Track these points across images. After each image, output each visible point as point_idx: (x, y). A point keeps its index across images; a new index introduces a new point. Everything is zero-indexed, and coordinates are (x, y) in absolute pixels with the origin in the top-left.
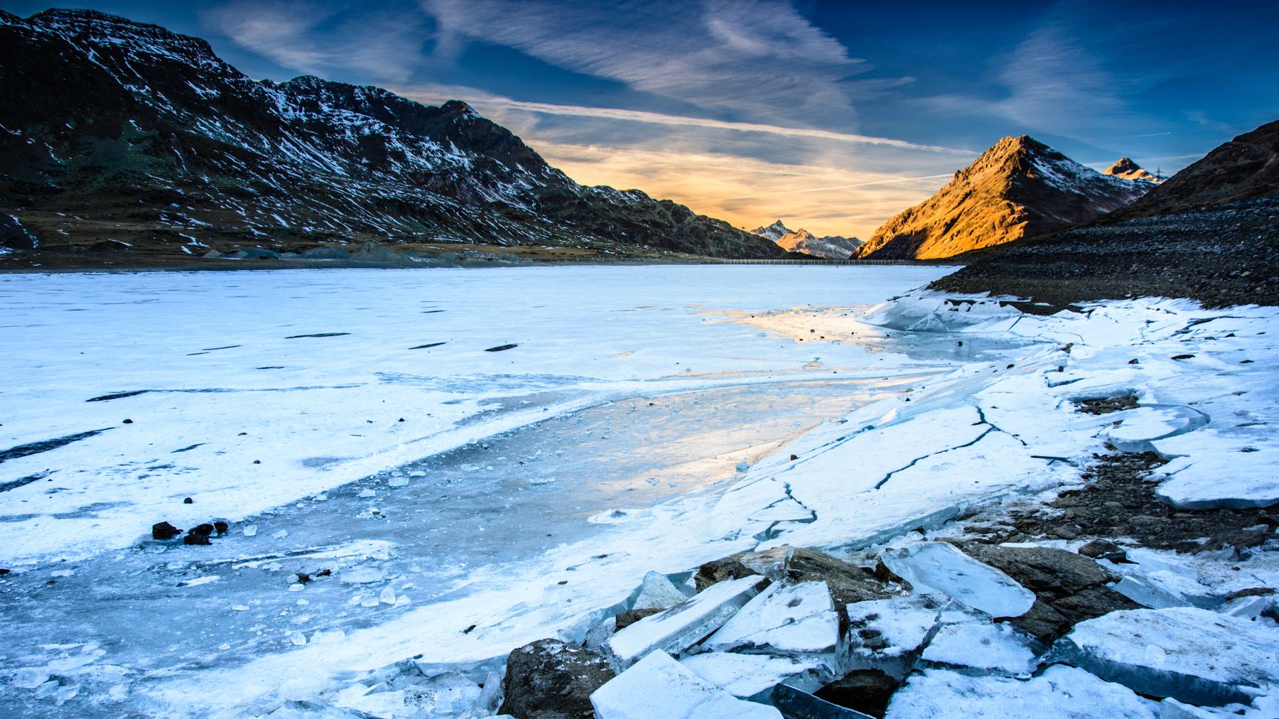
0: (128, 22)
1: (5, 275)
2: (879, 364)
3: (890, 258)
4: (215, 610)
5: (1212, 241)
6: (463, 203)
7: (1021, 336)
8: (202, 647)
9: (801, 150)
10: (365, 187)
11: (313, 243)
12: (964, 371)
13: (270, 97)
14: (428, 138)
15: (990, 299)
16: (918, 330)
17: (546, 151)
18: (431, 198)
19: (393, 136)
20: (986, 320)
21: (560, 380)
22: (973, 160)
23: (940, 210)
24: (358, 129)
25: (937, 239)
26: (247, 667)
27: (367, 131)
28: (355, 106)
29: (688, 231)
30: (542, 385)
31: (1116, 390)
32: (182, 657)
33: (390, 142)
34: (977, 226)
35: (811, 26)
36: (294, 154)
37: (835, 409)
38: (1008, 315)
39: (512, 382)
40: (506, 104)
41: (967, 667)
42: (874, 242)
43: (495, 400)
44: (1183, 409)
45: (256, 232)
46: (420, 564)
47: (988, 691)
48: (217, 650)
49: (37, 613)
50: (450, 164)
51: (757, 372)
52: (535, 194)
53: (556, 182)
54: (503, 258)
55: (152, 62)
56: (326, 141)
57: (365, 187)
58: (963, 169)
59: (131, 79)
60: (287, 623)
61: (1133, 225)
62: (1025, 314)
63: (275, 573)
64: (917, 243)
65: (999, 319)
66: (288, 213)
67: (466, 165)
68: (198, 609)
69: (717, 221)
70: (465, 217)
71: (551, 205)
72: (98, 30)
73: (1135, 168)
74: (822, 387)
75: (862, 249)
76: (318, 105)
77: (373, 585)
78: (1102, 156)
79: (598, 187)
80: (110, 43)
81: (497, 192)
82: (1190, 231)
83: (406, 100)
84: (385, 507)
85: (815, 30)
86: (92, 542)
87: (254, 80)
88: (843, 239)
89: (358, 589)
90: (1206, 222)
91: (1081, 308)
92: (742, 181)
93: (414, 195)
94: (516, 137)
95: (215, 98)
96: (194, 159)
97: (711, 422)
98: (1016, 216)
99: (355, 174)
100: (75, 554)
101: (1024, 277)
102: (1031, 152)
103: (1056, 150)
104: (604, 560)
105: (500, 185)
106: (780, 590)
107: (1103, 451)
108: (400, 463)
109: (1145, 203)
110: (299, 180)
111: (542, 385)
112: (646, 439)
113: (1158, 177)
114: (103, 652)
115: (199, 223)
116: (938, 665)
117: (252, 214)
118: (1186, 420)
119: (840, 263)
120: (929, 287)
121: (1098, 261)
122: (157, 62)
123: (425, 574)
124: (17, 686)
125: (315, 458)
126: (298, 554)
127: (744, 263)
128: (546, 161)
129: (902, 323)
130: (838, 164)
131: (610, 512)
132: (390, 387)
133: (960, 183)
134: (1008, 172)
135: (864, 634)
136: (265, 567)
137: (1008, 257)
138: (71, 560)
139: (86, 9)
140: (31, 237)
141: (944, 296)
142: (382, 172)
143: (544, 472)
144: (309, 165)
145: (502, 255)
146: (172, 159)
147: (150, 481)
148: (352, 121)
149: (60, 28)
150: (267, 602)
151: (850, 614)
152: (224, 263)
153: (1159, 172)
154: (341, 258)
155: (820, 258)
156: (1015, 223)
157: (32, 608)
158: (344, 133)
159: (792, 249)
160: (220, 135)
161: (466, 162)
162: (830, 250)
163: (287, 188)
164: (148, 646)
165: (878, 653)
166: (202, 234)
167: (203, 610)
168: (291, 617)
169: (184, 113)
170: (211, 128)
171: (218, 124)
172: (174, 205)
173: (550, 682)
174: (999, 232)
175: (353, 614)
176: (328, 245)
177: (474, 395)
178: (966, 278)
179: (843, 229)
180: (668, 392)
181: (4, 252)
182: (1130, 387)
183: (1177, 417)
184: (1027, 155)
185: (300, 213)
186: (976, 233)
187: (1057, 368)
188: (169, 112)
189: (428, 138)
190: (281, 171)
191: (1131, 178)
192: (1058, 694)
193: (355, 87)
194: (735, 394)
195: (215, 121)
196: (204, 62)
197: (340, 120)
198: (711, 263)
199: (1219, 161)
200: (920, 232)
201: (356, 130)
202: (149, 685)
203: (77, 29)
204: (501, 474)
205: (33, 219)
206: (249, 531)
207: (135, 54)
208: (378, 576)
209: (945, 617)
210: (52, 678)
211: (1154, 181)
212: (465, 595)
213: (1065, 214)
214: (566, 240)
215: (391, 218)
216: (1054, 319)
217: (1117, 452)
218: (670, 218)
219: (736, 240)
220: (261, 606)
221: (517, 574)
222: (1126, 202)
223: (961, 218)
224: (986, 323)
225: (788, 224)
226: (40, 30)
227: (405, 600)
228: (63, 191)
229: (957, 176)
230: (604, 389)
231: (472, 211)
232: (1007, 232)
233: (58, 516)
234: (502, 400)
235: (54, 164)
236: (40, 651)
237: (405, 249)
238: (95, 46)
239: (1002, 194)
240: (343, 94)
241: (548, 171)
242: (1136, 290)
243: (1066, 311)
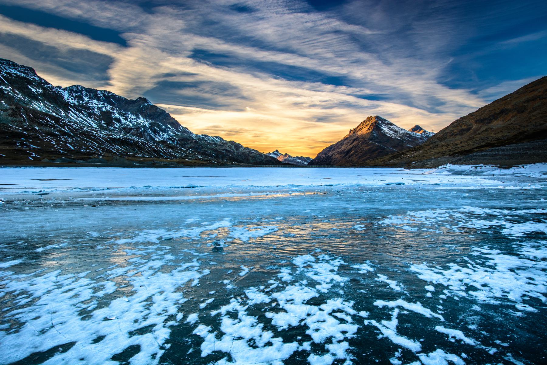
14: (129, 113)
19: (115, 111)
23: (344, 146)
27: (104, 109)
28: (98, 99)
33: (114, 114)
54: (171, 164)
55: (12, 77)
66: (74, 143)
67: (147, 125)
70: (150, 147)
71: (183, 142)
76: (83, 98)
79: (202, 135)
81: (160, 136)
83: (120, 97)
88: (304, 158)
96: (31, 119)
105: (161, 133)
109: (428, 143)
110: (78, 129)
115: (35, 147)
117: (58, 143)
122: (15, 77)
148: (98, 105)
158: (94, 110)
161: (147, 124)
162: (298, 162)
163: (73, 133)
166: (36, 151)
169: (27, 99)
170: (39, 106)
171: (42, 104)
188: (20, 98)
189: (129, 113)
195: (41, 103)
197: (92, 104)
199: (455, 127)
201: (99, 109)
207: (5, 73)
215: (118, 147)
218: (234, 149)
222: (418, 142)
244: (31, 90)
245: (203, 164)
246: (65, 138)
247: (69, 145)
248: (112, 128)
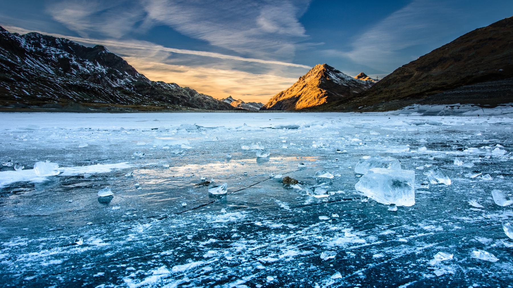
14: (87, 60)
18: (91, 85)
19: (73, 59)
23: (294, 92)
24: (58, 55)
27: (62, 56)
28: (56, 46)
33: (72, 61)
45: (16, 97)
50: (97, 71)
52: (133, 84)
54: (127, 110)
56: (45, 60)
66: (30, 89)
67: (104, 72)
71: (140, 89)
73: (366, 76)
79: (158, 82)
81: (117, 83)
83: (78, 44)
88: (256, 103)
98: (323, 94)
99: (58, 74)
102: (328, 70)
105: (118, 80)
109: (373, 89)
110: (34, 75)
117: (13, 88)
128: (137, 70)
133: (302, 82)
134: (319, 77)
144: (38, 69)
145: (126, 108)
148: (55, 52)
154: (58, 108)
156: (323, 97)
158: (52, 57)
161: (104, 70)
162: (251, 108)
163: (29, 79)
174: (317, 100)
185: (34, 89)
189: (87, 60)
190: (26, 71)
191: (365, 80)
197: (50, 51)
199: (398, 74)
214: (148, 103)
215: (75, 93)
218: (189, 95)
219: (215, 103)
229: (300, 79)
231: (109, 90)
240: (51, 41)
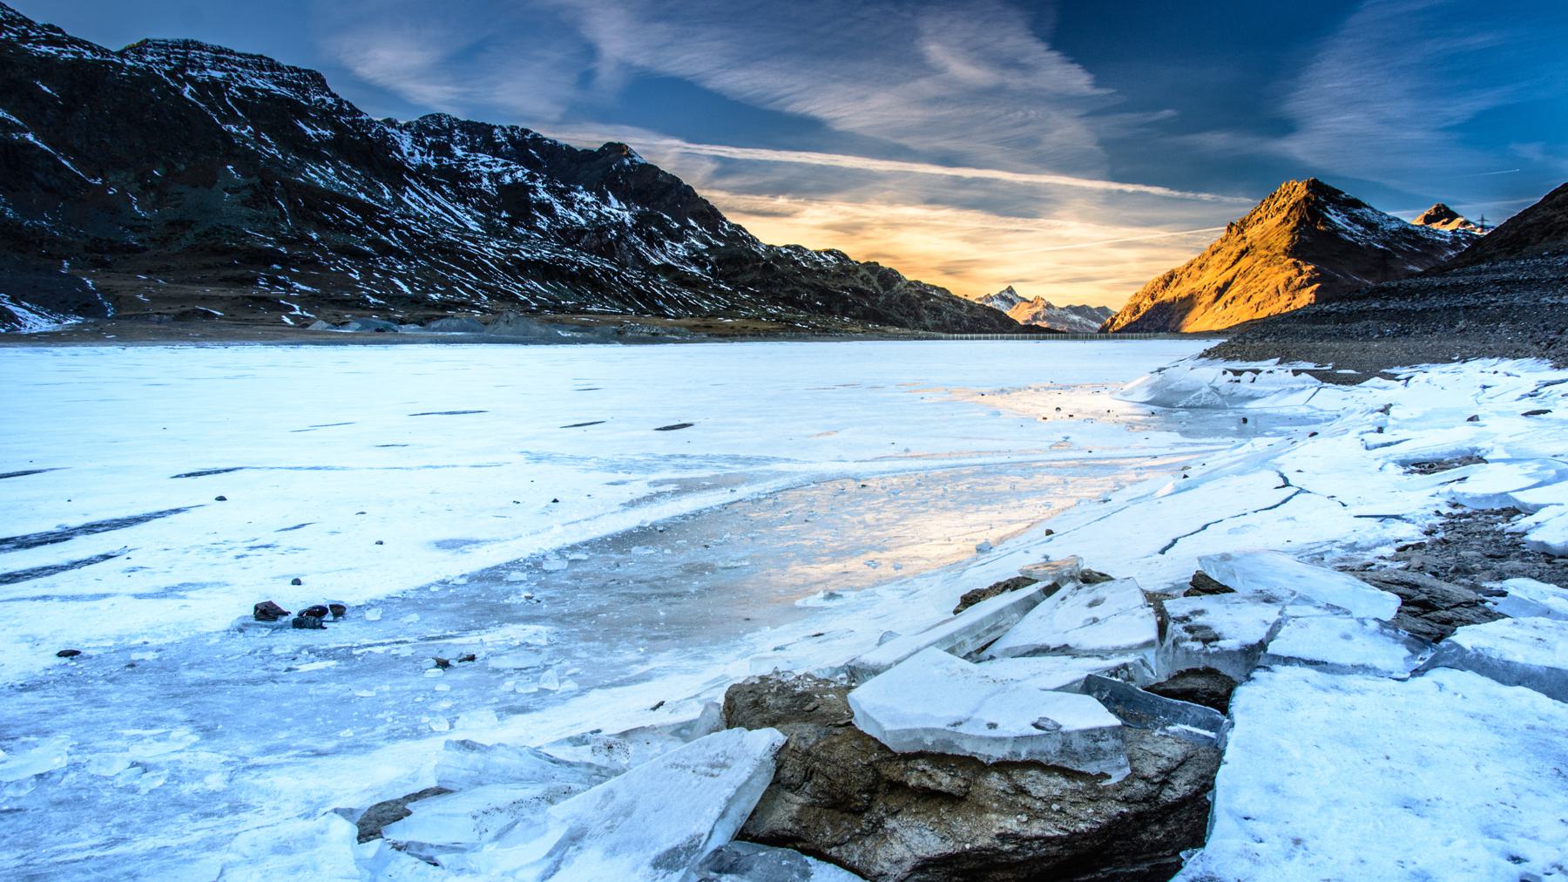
0: (231, 52)
1: (73, 348)
2: (1145, 443)
3: (1149, 331)
4: (335, 696)
5: (1559, 291)
6: (622, 266)
7: (1321, 410)
8: (317, 735)
9: (1038, 200)
10: (505, 245)
11: (440, 314)
12: (1253, 445)
13: (393, 139)
14: (581, 188)
15: (1280, 367)
16: (1191, 407)
17: (726, 202)
18: (583, 260)
19: (539, 185)
20: (1276, 392)
21: (748, 461)
22: (1249, 210)
23: (1210, 271)
25: (1206, 308)
26: (376, 753)
27: (507, 179)
28: (495, 150)
29: (898, 299)
30: (727, 465)
31: (1453, 449)
32: (294, 745)
33: (535, 192)
34: (1256, 290)
35: (1049, 50)
36: (420, 207)
37: (1094, 489)
38: (1303, 386)
39: (689, 462)
40: (678, 146)
41: (1326, 663)
42: (1128, 312)
43: (670, 481)
44: (1544, 462)
46: (587, 650)
47: (1357, 688)
48: (338, 737)
49: (114, 698)
51: (993, 452)
53: (736, 240)
54: (671, 333)
55: (257, 99)
56: (458, 191)
57: (505, 245)
58: (1237, 221)
59: (231, 117)
60: (424, 710)
61: (1457, 275)
62: (1325, 384)
63: (406, 659)
64: (1182, 313)
65: (1292, 391)
66: (411, 276)
67: (627, 220)
68: (311, 696)
69: (935, 288)
71: (729, 268)
72: (196, 62)
74: (1075, 467)
75: (1113, 320)
77: (530, 670)
78: (1411, 202)
79: (787, 247)
80: (210, 77)
81: (664, 252)
82: (1530, 280)
83: (556, 142)
84: (539, 591)
85: (1054, 55)
86: (180, 624)
87: (375, 119)
88: (1090, 309)
89: (510, 675)
90: (1550, 268)
91: (1396, 375)
92: (965, 239)
93: (563, 256)
94: (688, 186)
95: (328, 140)
96: (300, 211)
97: (940, 504)
98: (1305, 277)
99: (493, 231)
100: (160, 636)
101: (1321, 340)
103: (1353, 196)
104: (821, 638)
105: (667, 243)
106: (1075, 591)
107: (1445, 510)
108: (558, 544)
110: (424, 237)
111: (727, 465)
112: (860, 523)
113: (1482, 227)
114: (195, 738)
115: (305, 288)
116: (1288, 661)
118: (1552, 472)
119: (1086, 338)
120: (1201, 356)
121: (1414, 318)
122: (262, 98)
123: (594, 659)
124: (92, 773)
125: (451, 540)
126: (433, 638)
127: (967, 339)
128: (725, 215)
129: (1169, 399)
130: (1083, 216)
131: (821, 594)
132: (540, 466)
133: (1234, 238)
134: (1292, 224)
135: (1189, 630)
136: (394, 652)
137: (1301, 317)
138: (154, 642)
139: (184, 38)
140: (106, 303)
141: (1221, 365)
142: (525, 227)
143: (734, 556)
145: (670, 329)
146: (275, 212)
147: (249, 561)
148: (490, 167)
149: (153, 61)
150: (398, 688)
151: (1168, 610)
152: (333, 337)
153: (1483, 220)
154: (472, 331)
155: (1062, 332)
156: (1305, 287)
157: (108, 692)
158: (481, 181)
159: (1027, 321)
160: (333, 183)
161: (627, 216)
162: (1074, 323)
164: (251, 732)
165: (1212, 647)
166: (307, 301)
167: (317, 696)
168: (429, 704)
169: (291, 157)
170: (322, 175)
171: (330, 170)
172: (275, 266)
173: (788, 700)
175: (505, 701)
176: (458, 315)
177: (643, 476)
178: (1248, 342)
179: (1089, 295)
180: (884, 473)
181: (74, 321)
182: (1472, 445)
183: (1539, 469)
184: (1316, 202)
186: (1256, 299)
187: (1375, 428)
188: (274, 156)
189: (581, 188)
190: (403, 226)
191: (1448, 229)
192: (1446, 695)
193: (495, 127)
194: (967, 476)
195: (327, 167)
196: (317, 98)
197: (476, 165)
198: (927, 339)
199: (1559, 206)
200: (1186, 299)
202: (254, 772)
203: (173, 62)
204: (682, 558)
205: (109, 282)
206: (372, 615)
207: (237, 89)
208: (535, 661)
209: (1290, 611)
210: (134, 765)
211: (1477, 232)
212: (648, 680)
213: (1367, 274)
214: (749, 311)
215: (535, 284)
216: (1362, 389)
217: (1465, 509)
218: (876, 284)
219: (957, 311)
220: (390, 692)
221: (710, 658)
223: (1236, 280)
224: (1276, 396)
225: (1021, 290)
226: (132, 64)
227: (570, 685)
228: (145, 249)
229: (1229, 229)
230: (804, 469)
231: (633, 276)
232: (1294, 298)
233: (138, 596)
234: (678, 481)
235: (137, 218)
236: (119, 737)
237: (551, 321)
238: (191, 80)
239: (1286, 250)
240: (480, 135)
241: (726, 227)
242: (1464, 351)
243: (1377, 379)
244: (303, 131)
245: (768, 330)
246: (388, 263)
247: (398, 282)
248: (522, 231)
